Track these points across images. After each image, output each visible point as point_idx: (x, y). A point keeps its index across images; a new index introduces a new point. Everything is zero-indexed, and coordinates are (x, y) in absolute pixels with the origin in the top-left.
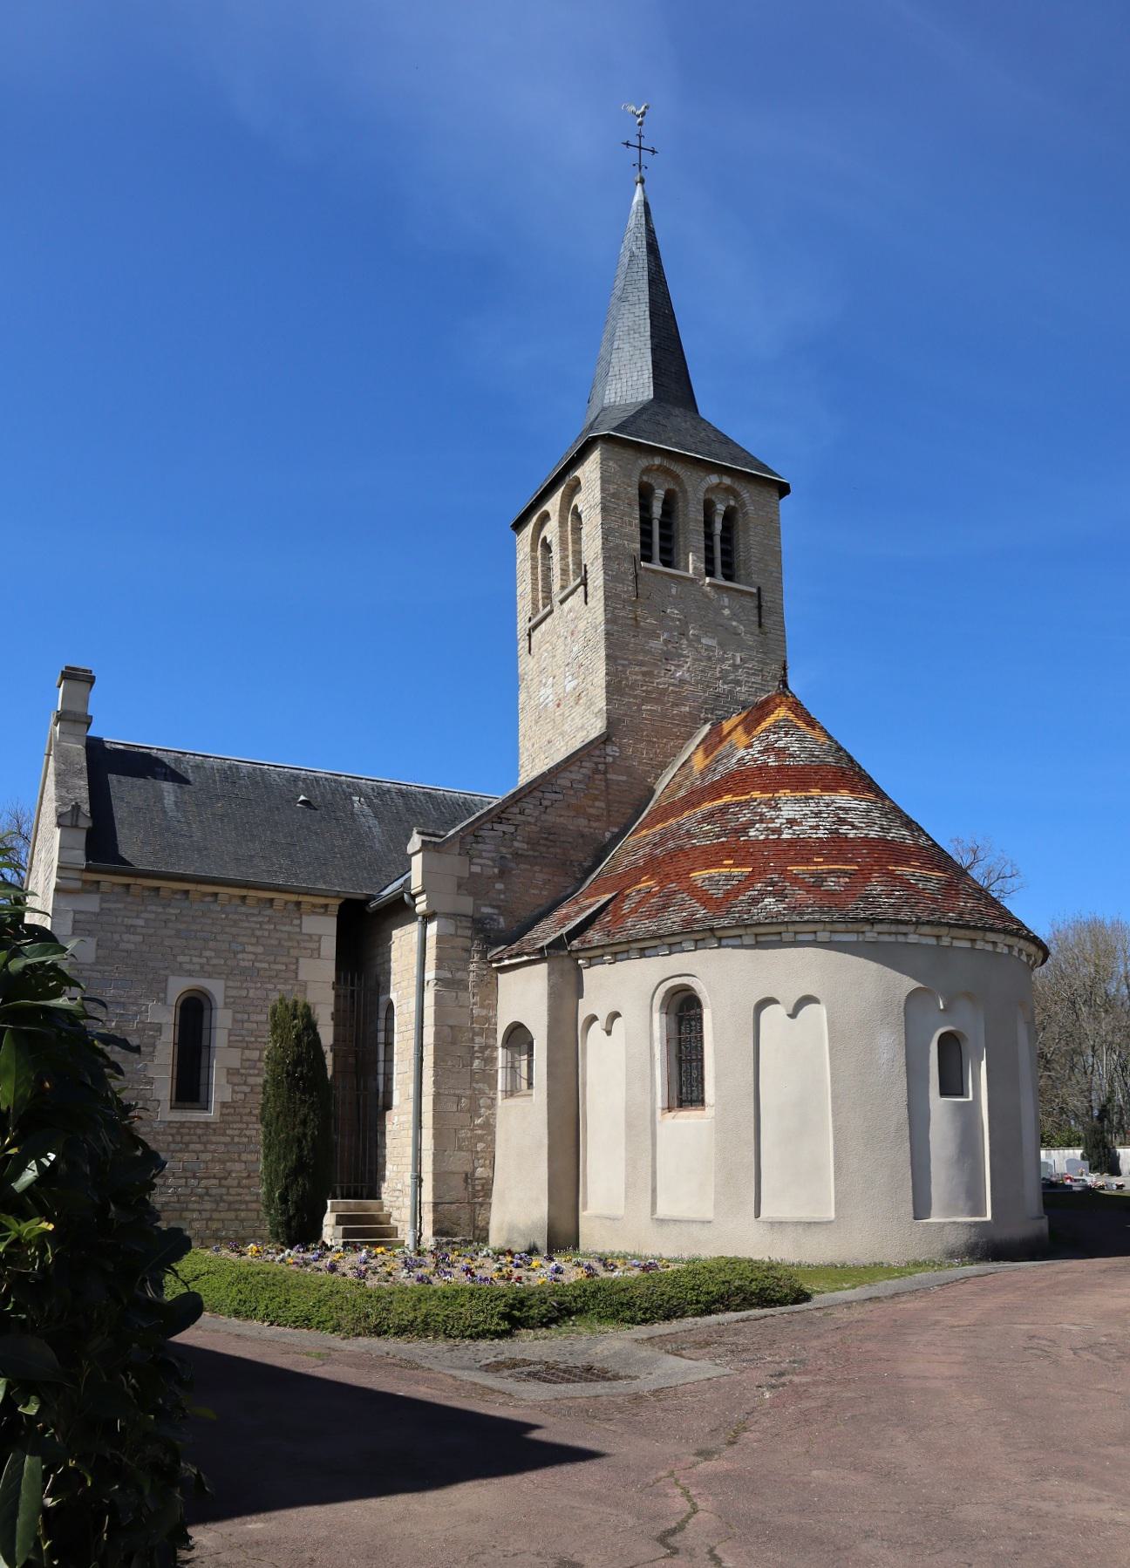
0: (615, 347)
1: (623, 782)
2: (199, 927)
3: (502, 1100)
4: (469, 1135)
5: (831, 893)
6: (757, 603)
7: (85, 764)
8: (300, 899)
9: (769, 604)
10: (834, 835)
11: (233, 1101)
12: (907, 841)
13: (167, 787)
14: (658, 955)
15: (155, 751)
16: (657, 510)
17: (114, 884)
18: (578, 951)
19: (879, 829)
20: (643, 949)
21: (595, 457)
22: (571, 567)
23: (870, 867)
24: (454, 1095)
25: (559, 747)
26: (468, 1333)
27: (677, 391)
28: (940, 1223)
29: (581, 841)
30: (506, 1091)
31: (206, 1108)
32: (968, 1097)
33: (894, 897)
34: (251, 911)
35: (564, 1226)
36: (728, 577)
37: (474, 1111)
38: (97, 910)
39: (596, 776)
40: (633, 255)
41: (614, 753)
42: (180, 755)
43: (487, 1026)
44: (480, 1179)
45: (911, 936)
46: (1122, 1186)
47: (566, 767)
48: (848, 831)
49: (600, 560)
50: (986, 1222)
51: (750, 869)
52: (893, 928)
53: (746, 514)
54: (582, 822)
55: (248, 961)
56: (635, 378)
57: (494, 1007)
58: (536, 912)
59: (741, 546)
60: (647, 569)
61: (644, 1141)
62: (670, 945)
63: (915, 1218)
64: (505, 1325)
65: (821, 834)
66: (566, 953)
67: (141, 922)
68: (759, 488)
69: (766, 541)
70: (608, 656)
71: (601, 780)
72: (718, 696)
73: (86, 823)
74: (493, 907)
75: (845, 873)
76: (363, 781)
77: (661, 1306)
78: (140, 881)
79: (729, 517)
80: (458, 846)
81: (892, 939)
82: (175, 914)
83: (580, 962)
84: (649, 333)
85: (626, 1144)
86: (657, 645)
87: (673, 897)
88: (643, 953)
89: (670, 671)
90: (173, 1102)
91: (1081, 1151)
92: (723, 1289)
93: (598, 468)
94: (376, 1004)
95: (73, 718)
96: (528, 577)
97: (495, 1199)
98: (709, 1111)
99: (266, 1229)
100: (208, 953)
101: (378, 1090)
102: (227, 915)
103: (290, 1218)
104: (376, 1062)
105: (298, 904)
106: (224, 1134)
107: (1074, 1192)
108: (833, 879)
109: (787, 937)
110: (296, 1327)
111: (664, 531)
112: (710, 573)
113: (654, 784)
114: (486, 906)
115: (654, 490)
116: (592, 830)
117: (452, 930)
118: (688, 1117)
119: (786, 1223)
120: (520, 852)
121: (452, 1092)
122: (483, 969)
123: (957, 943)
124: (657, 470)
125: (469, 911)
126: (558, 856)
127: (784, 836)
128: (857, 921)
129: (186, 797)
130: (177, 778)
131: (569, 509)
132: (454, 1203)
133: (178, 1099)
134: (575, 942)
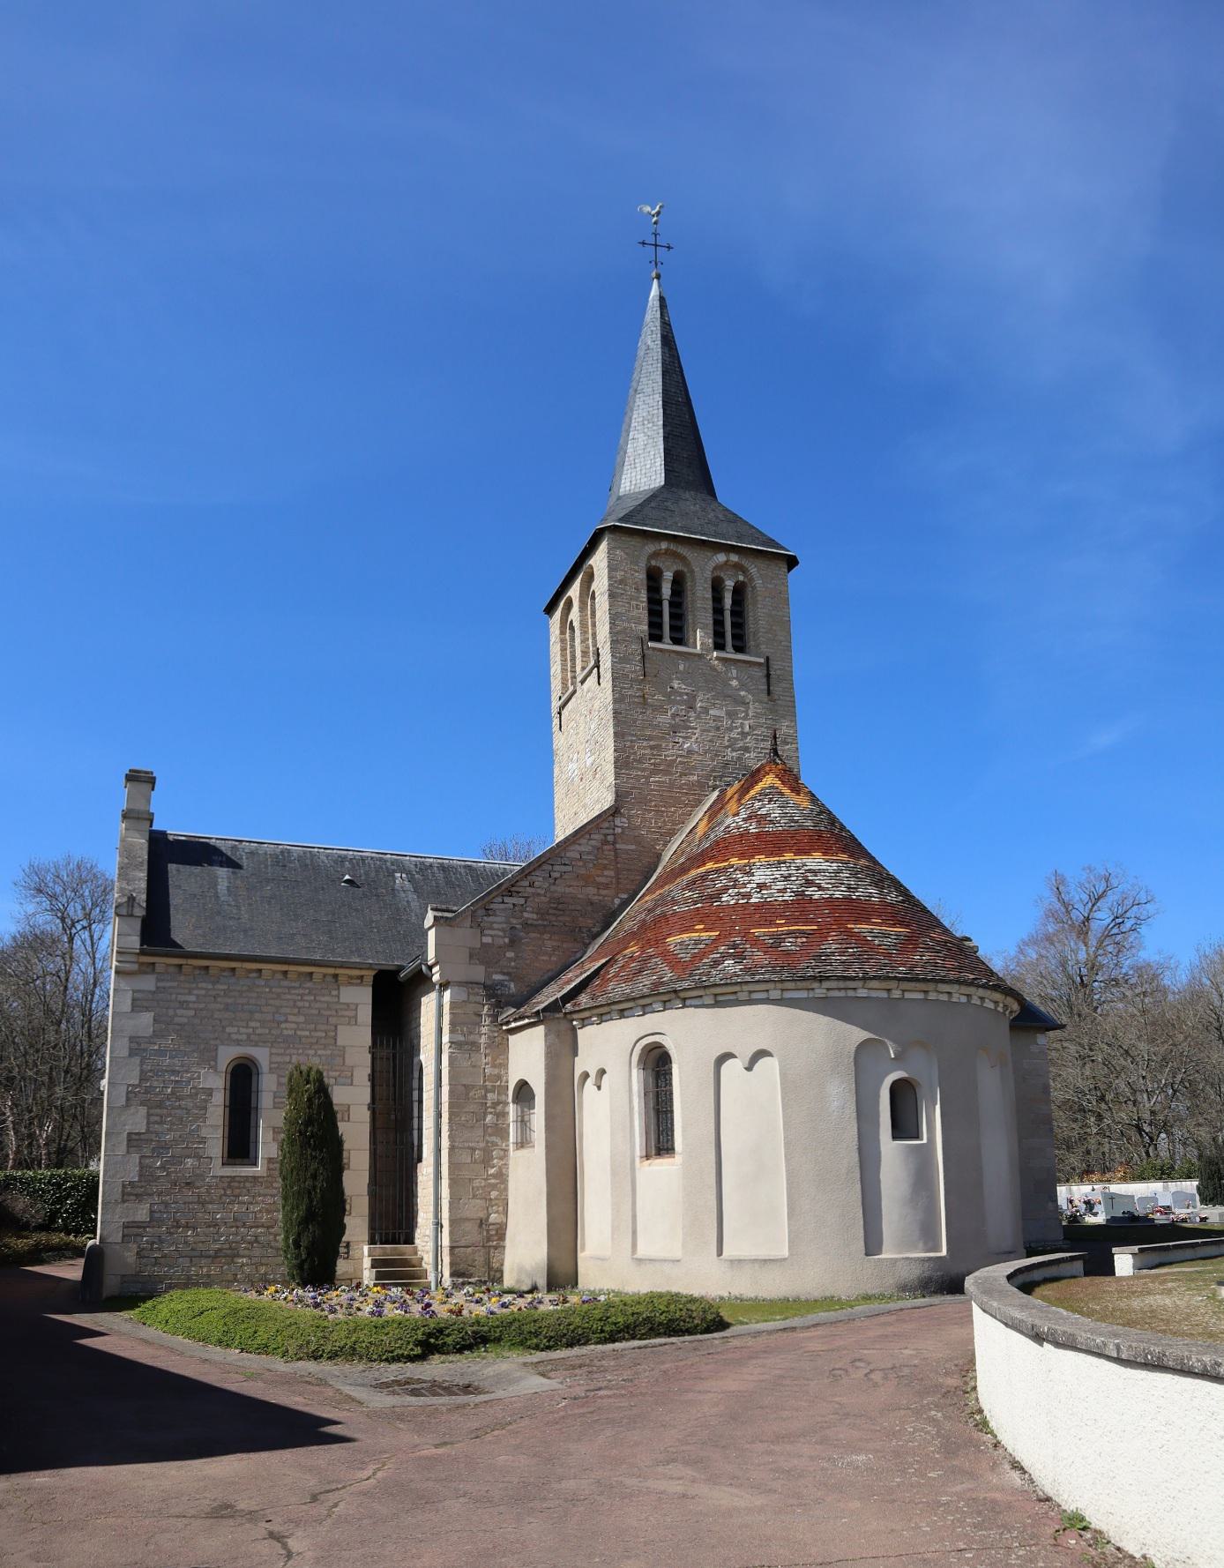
0: (631, 437)
1: (632, 850)
2: (245, 1001)
4: (483, 1184)
5: (788, 953)
6: (765, 672)
7: (146, 857)
9: (778, 672)
10: (800, 897)
12: (873, 899)
13: (222, 872)
15: (214, 841)
16: (666, 591)
17: (168, 965)
18: (571, 1013)
21: (603, 547)
23: (829, 927)
24: (469, 1148)
26: (384, 1357)
27: (688, 475)
29: (589, 908)
30: (517, 1143)
31: (255, 1164)
32: (922, 1140)
33: (846, 954)
34: (293, 984)
35: (563, 1268)
36: (739, 649)
37: (486, 1161)
38: (154, 989)
39: (605, 847)
42: (237, 843)
43: (498, 1083)
44: (494, 1224)
45: (860, 991)
46: (1206, 1218)
48: (813, 893)
50: (941, 1257)
51: (717, 933)
52: (841, 984)
53: (754, 588)
55: (291, 1029)
56: (648, 466)
57: (505, 1066)
58: (546, 977)
59: (751, 618)
60: (654, 649)
61: (626, 1187)
63: (867, 1254)
64: (418, 1351)
65: (788, 896)
66: (561, 1015)
67: (193, 998)
68: (768, 562)
69: (773, 613)
70: (616, 734)
71: (610, 850)
72: (726, 764)
73: (140, 912)
74: (504, 974)
75: (803, 932)
76: (408, 858)
77: (565, 1335)
78: (190, 961)
79: (739, 591)
81: (842, 994)
82: (224, 990)
83: (575, 1023)
84: (661, 422)
85: (612, 1189)
86: (664, 719)
88: (622, 1014)
89: (678, 743)
90: (225, 1159)
91: (1197, 1183)
92: (631, 1320)
95: (137, 816)
96: (558, 658)
97: (508, 1242)
98: (678, 1159)
99: (284, 1269)
100: (252, 1024)
101: (413, 1144)
102: (271, 988)
103: (303, 1262)
105: (336, 976)
107: (1156, 1226)
108: (791, 940)
109: (743, 996)
110: (259, 1354)
111: (674, 610)
112: (719, 646)
113: (663, 850)
115: (662, 572)
116: (601, 898)
117: (464, 997)
119: (745, 1260)
120: (529, 922)
122: (494, 1031)
123: (907, 995)
124: (666, 553)
125: (481, 977)
127: (753, 900)
128: (804, 979)
129: (239, 882)
130: (231, 864)
134: (568, 1006)
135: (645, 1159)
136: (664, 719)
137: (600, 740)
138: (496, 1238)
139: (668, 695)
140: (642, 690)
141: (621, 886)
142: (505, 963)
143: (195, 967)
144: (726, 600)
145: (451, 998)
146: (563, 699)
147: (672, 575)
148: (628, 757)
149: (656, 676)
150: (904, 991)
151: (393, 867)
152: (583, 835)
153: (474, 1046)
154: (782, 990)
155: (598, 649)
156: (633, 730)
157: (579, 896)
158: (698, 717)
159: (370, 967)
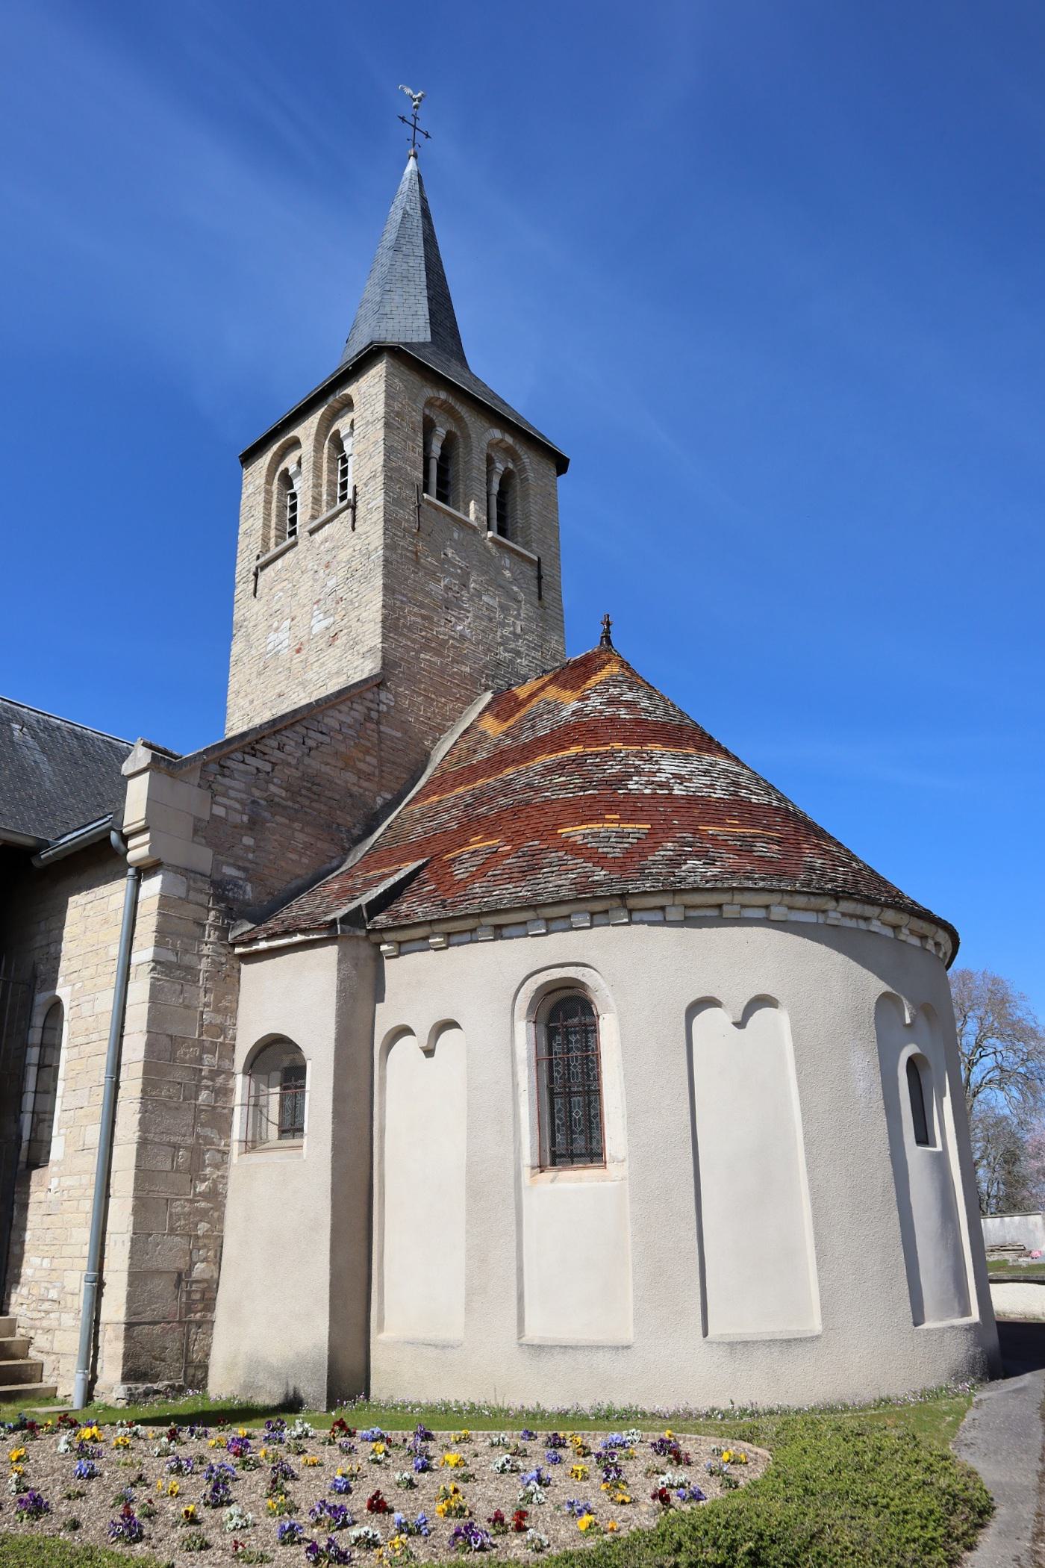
3: (240, 1154)
14: (527, 935)
20: (498, 927)
22: (325, 497)
28: (938, 1329)
29: (349, 801)
35: (350, 1361)
37: (195, 1172)
39: (368, 724)
40: (406, 215)
43: (221, 1040)
47: (337, 704)
49: (380, 479)
51: (649, 826)
54: (351, 778)
57: (232, 1012)
58: (293, 885)
62: (548, 920)
66: (362, 933)
74: (239, 868)
79: (507, 479)
80: (199, 774)
86: (438, 588)
88: (499, 932)
94: (27, 1007)
96: (259, 512)
97: (221, 1314)
101: (20, 1137)
104: (21, 1093)
114: (229, 864)
115: (435, 426)
116: (361, 791)
118: (580, 1180)
120: (277, 799)
121: (166, 1138)
126: (322, 815)
131: (326, 436)
132: (160, 1323)
135: (538, 1170)
136: (438, 588)
138: (200, 1306)
139: (443, 562)
140: (416, 545)
141: (384, 782)
142: (241, 852)
145: (162, 888)
146: (262, 560)
148: (398, 619)
152: (344, 700)
153: (191, 971)
156: (404, 589)
157: (337, 781)
158: (470, 599)
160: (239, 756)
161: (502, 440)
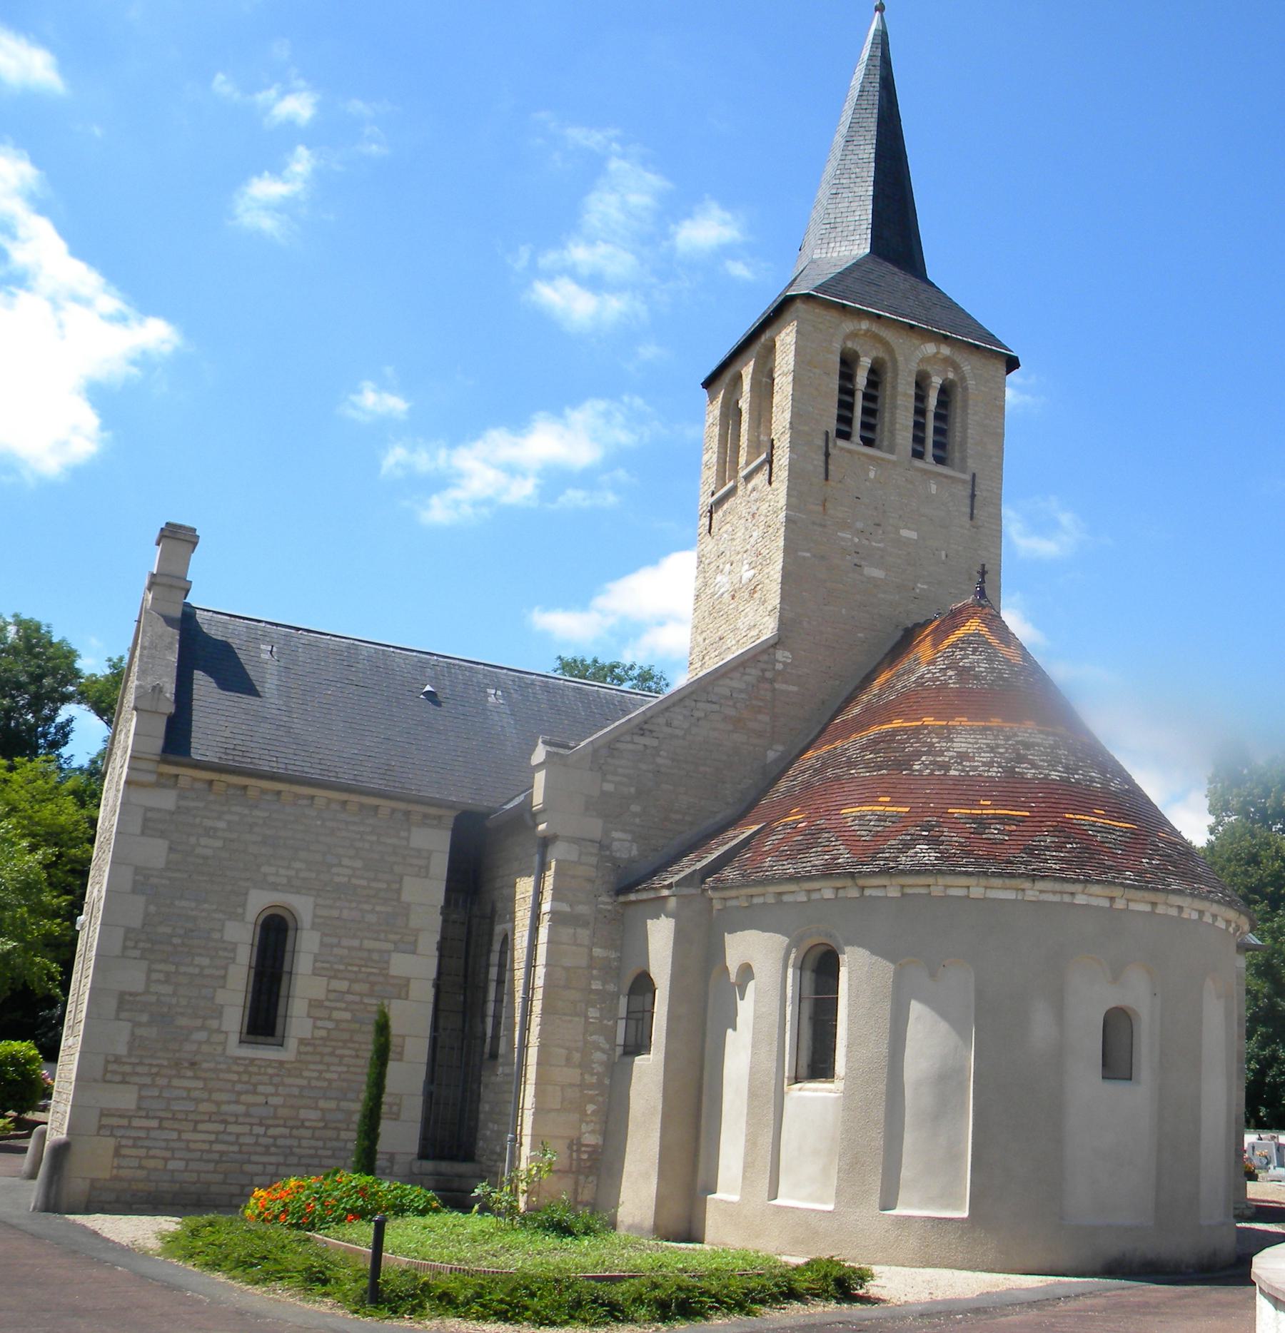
8: (410, 809)
11: (313, 1038)
16: (861, 380)
17: (195, 779)
19: (1062, 770)
25: (729, 646)
41: (784, 659)
51: (907, 809)
53: (965, 389)
60: (842, 449)
67: (222, 825)
78: (224, 777)
79: (945, 391)
87: (819, 835)
93: (794, 331)
94: (491, 934)
100: (298, 865)
101: (485, 1034)
104: (485, 1002)
105: (407, 814)
106: (301, 1076)
123: (1133, 906)
124: (865, 335)
127: (952, 773)
133: (249, 1033)
137: (764, 552)
143: (229, 785)
144: (930, 399)
147: (870, 361)
149: (840, 482)
150: (1128, 900)
151: (485, 681)
154: (986, 888)
155: (773, 440)
159: (451, 806)
160: (628, 738)
161: (938, 353)
